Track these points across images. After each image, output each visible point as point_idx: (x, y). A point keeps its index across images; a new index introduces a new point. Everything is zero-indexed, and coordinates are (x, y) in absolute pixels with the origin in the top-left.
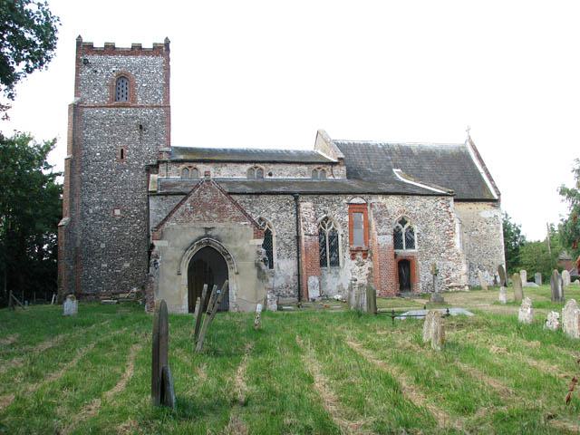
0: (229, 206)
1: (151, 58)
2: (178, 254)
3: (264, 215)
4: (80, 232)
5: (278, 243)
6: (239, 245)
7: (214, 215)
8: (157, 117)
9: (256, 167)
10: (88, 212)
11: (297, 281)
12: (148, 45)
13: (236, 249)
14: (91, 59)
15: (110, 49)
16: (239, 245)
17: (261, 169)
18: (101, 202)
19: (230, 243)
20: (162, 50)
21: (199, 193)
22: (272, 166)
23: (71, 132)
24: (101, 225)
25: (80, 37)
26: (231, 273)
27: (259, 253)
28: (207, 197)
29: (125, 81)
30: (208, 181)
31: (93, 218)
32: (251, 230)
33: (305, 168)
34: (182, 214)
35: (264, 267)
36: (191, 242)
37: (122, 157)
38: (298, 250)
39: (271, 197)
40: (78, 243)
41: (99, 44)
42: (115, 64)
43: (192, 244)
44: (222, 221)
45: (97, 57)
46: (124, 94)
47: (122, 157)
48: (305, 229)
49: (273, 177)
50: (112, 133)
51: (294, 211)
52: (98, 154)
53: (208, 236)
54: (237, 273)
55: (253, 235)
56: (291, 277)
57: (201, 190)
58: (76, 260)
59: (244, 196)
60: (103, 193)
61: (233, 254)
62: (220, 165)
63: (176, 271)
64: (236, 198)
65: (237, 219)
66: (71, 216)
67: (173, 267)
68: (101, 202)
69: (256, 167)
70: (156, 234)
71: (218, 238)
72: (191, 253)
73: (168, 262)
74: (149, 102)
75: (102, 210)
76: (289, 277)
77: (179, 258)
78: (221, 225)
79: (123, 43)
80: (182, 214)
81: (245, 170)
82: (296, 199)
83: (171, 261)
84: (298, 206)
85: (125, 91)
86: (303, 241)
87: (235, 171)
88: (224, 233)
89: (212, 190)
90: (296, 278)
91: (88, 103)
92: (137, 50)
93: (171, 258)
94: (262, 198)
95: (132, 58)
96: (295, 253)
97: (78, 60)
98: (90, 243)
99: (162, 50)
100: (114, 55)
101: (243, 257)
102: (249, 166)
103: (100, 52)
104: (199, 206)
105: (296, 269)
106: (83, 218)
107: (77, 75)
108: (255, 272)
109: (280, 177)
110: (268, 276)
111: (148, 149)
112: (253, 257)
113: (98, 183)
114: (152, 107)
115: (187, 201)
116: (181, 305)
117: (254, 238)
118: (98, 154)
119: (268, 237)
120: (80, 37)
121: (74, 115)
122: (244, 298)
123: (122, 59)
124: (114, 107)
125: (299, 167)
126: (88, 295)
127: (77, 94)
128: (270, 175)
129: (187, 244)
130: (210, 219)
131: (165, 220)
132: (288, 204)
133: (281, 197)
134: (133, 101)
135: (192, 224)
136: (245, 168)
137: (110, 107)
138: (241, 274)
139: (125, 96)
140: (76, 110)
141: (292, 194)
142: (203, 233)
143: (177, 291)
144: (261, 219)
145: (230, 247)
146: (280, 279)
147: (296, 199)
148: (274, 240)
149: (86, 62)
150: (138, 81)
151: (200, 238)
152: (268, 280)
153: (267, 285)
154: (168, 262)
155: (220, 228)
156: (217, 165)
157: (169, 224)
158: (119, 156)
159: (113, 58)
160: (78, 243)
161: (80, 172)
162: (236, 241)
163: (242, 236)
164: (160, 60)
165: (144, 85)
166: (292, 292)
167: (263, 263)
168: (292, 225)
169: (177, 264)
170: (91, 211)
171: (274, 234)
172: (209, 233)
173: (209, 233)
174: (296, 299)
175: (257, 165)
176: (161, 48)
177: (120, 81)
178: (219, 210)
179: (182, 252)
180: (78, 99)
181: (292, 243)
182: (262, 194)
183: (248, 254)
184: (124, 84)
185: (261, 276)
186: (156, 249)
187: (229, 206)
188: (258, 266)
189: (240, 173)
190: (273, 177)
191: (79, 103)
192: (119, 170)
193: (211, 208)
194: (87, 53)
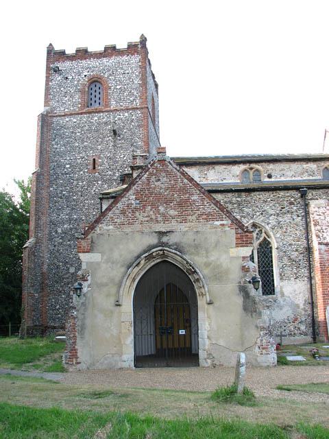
0: (195, 197)
1: (125, 58)
2: (118, 272)
3: (259, 220)
4: (47, 255)
5: (280, 259)
6: (213, 257)
7: (172, 212)
8: (132, 121)
9: (251, 169)
10: (56, 232)
11: (309, 312)
12: (122, 45)
13: (207, 265)
14: (64, 65)
15: (83, 54)
16: (213, 257)
17: (257, 170)
18: (70, 220)
19: (198, 254)
20: (139, 48)
21: (148, 179)
22: (271, 166)
23: (39, 144)
24: (70, 246)
25: (51, 45)
26: (201, 302)
27: (245, 269)
28: (161, 184)
29: (98, 85)
30: (162, 161)
31: (62, 238)
32: (232, 234)
33: (313, 166)
34: (123, 212)
35: (253, 292)
36: (136, 255)
37: (94, 168)
38: (310, 268)
39: (267, 194)
40: (45, 266)
41: (70, 51)
42: (86, 69)
43: (139, 257)
44: (185, 221)
45: (68, 64)
46: (97, 99)
47: (94, 168)
48: (318, 236)
49: (273, 180)
50: (83, 141)
51: (301, 212)
52: (68, 166)
53: (166, 245)
54: (209, 304)
55: (234, 241)
56: (302, 306)
57: (151, 174)
58: (43, 286)
59: (230, 195)
60: (73, 209)
61: (203, 272)
62: (206, 168)
63: (112, 300)
64: (219, 197)
65: (209, 217)
66: (37, 237)
67: (108, 296)
68: (70, 220)
69: (251, 169)
70: (84, 244)
71: (179, 248)
72: (138, 272)
73: (101, 286)
74: (124, 105)
75: (71, 229)
76: (298, 306)
77: (117, 280)
78: (183, 227)
79: (96, 47)
80: (123, 212)
81: (238, 173)
82: (303, 195)
83: (106, 285)
84: (307, 205)
85: (98, 96)
86: (316, 255)
87: (225, 174)
88: (187, 240)
89: (168, 174)
90: (308, 308)
91: (57, 112)
92: (111, 51)
93: (105, 280)
94: (256, 195)
95: (105, 60)
96: (305, 272)
97: (48, 68)
98: (58, 267)
99: (139, 48)
100: (85, 59)
101: (219, 275)
102: (242, 167)
103: (71, 58)
104: (148, 199)
105: (307, 295)
106: (51, 239)
107: (47, 84)
108: (239, 300)
109: (283, 179)
110: (260, 307)
111: (124, 157)
112: (235, 275)
113: (67, 198)
114: (127, 109)
115: (131, 192)
116: (120, 354)
117: (238, 245)
118: (68, 166)
119: (265, 250)
120: (51, 45)
121: (42, 127)
122: (222, 342)
123: (92, 63)
124: (85, 113)
125: (305, 166)
126: (55, 328)
127: (46, 103)
128: (270, 176)
129: (129, 257)
130: (166, 218)
131: (97, 221)
132: (291, 203)
133: (282, 193)
134: (107, 106)
135: (137, 226)
136: (238, 169)
137: (81, 114)
138: (217, 304)
139: (98, 101)
140: (45, 121)
141: (296, 188)
142: (154, 240)
143: (115, 332)
144: (254, 225)
145: (197, 260)
146: (285, 310)
147: (303, 195)
148: (275, 254)
149: (57, 70)
150: (112, 84)
151: (151, 247)
152: (260, 314)
153: (260, 323)
154: (101, 286)
155: (182, 232)
156: (202, 168)
157: (103, 227)
158: (91, 167)
159: (84, 63)
160: (45, 266)
161: (48, 187)
162: (207, 252)
163: (217, 244)
164: (135, 59)
165: (118, 87)
166: (303, 328)
167: (251, 286)
168: (300, 232)
169: (113, 290)
170: (59, 231)
171: (274, 245)
172: (165, 239)
173: (165, 239)
174: (309, 339)
175: (253, 165)
176: (136, 46)
177: (93, 86)
178: (180, 205)
179: (123, 270)
180: (48, 108)
181: (301, 257)
182: (254, 190)
183: (227, 272)
184: (97, 88)
185: (250, 307)
186: (84, 266)
187: (195, 197)
188: (243, 290)
189: (232, 176)
190: (273, 180)
191: (48, 112)
192: (90, 183)
193: (168, 202)
194: (58, 61)
